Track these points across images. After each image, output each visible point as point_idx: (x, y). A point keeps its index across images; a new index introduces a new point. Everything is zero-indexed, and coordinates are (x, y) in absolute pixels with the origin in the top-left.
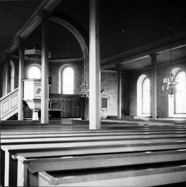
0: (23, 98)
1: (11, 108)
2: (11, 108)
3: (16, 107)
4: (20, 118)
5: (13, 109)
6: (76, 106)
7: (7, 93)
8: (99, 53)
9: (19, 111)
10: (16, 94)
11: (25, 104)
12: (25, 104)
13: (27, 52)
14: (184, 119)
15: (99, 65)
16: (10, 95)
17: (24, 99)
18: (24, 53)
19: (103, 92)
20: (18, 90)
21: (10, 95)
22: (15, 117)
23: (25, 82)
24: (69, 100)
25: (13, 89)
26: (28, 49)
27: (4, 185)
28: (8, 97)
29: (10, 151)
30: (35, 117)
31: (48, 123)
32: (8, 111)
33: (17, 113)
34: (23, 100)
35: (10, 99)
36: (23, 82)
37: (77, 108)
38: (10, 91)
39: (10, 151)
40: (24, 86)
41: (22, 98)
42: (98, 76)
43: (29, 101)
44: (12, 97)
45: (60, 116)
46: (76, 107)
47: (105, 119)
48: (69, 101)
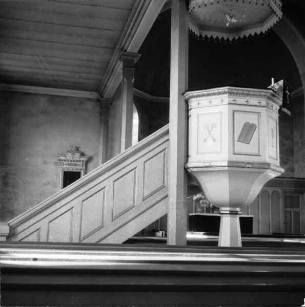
0: (187, 161)
1: (113, 220)
2: (113, 220)
5: (152, 201)
6: (286, 207)
8: (16, 267)
9: (173, 209)
10: (131, 167)
11: (191, 184)
12: (191, 184)
15: (186, 188)
17: (190, 165)
20: (167, 133)
22: (161, 224)
23: (193, 103)
25: (124, 149)
28: (101, 178)
31: (240, 245)
32: (101, 227)
34: (186, 169)
35: (139, 164)
36: (187, 102)
37: (291, 212)
38: (120, 153)
40: (188, 117)
43: (210, 170)
44: (117, 176)
45: (251, 232)
46: (288, 209)
48: (270, 193)
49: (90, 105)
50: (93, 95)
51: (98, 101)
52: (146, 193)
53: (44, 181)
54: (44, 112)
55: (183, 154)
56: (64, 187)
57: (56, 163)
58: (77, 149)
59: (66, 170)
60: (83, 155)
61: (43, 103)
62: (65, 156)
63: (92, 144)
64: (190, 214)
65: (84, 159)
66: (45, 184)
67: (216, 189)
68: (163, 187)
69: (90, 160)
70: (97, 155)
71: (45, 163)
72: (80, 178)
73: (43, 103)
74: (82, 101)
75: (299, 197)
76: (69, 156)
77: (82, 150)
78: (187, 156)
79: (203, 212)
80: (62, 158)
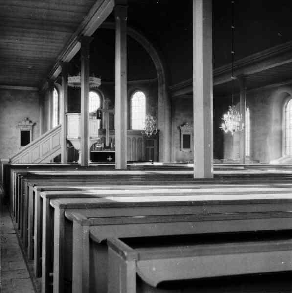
3: (58, 147)
4: (63, 162)
5: (55, 150)
7: (42, 134)
8: (210, 33)
9: (63, 152)
13: (70, 79)
14: (122, 290)
16: (45, 136)
18: (67, 80)
19: (185, 126)
20: (39, 146)
21: (45, 136)
23: (68, 116)
24: (137, 137)
26: (72, 76)
27: (290, 230)
29: (61, 206)
30: (80, 162)
33: (60, 155)
34: (67, 139)
35: (51, 137)
36: (67, 116)
39: (61, 206)
41: (65, 136)
42: (124, 116)
47: (212, 179)
49: (33, 95)
50: (36, 89)
51: (38, 92)
52: (54, 147)
53: (10, 137)
54: (9, 99)
55: (65, 133)
56: (90, 235)
57: (16, 127)
58: (28, 119)
59: (22, 130)
60: (31, 122)
61: (8, 95)
62: (21, 123)
63: (37, 117)
64: (92, 152)
65: (32, 124)
66: (11, 138)
67: (77, 146)
68: (59, 145)
69: (35, 124)
70: (38, 121)
71: (11, 127)
72: (29, 143)
73: (8, 95)
74: (29, 92)
75: (153, 141)
76: (24, 123)
77: (31, 119)
78: (67, 134)
79: (97, 150)
80: (20, 124)
